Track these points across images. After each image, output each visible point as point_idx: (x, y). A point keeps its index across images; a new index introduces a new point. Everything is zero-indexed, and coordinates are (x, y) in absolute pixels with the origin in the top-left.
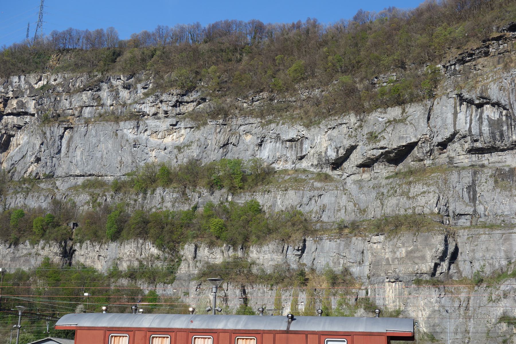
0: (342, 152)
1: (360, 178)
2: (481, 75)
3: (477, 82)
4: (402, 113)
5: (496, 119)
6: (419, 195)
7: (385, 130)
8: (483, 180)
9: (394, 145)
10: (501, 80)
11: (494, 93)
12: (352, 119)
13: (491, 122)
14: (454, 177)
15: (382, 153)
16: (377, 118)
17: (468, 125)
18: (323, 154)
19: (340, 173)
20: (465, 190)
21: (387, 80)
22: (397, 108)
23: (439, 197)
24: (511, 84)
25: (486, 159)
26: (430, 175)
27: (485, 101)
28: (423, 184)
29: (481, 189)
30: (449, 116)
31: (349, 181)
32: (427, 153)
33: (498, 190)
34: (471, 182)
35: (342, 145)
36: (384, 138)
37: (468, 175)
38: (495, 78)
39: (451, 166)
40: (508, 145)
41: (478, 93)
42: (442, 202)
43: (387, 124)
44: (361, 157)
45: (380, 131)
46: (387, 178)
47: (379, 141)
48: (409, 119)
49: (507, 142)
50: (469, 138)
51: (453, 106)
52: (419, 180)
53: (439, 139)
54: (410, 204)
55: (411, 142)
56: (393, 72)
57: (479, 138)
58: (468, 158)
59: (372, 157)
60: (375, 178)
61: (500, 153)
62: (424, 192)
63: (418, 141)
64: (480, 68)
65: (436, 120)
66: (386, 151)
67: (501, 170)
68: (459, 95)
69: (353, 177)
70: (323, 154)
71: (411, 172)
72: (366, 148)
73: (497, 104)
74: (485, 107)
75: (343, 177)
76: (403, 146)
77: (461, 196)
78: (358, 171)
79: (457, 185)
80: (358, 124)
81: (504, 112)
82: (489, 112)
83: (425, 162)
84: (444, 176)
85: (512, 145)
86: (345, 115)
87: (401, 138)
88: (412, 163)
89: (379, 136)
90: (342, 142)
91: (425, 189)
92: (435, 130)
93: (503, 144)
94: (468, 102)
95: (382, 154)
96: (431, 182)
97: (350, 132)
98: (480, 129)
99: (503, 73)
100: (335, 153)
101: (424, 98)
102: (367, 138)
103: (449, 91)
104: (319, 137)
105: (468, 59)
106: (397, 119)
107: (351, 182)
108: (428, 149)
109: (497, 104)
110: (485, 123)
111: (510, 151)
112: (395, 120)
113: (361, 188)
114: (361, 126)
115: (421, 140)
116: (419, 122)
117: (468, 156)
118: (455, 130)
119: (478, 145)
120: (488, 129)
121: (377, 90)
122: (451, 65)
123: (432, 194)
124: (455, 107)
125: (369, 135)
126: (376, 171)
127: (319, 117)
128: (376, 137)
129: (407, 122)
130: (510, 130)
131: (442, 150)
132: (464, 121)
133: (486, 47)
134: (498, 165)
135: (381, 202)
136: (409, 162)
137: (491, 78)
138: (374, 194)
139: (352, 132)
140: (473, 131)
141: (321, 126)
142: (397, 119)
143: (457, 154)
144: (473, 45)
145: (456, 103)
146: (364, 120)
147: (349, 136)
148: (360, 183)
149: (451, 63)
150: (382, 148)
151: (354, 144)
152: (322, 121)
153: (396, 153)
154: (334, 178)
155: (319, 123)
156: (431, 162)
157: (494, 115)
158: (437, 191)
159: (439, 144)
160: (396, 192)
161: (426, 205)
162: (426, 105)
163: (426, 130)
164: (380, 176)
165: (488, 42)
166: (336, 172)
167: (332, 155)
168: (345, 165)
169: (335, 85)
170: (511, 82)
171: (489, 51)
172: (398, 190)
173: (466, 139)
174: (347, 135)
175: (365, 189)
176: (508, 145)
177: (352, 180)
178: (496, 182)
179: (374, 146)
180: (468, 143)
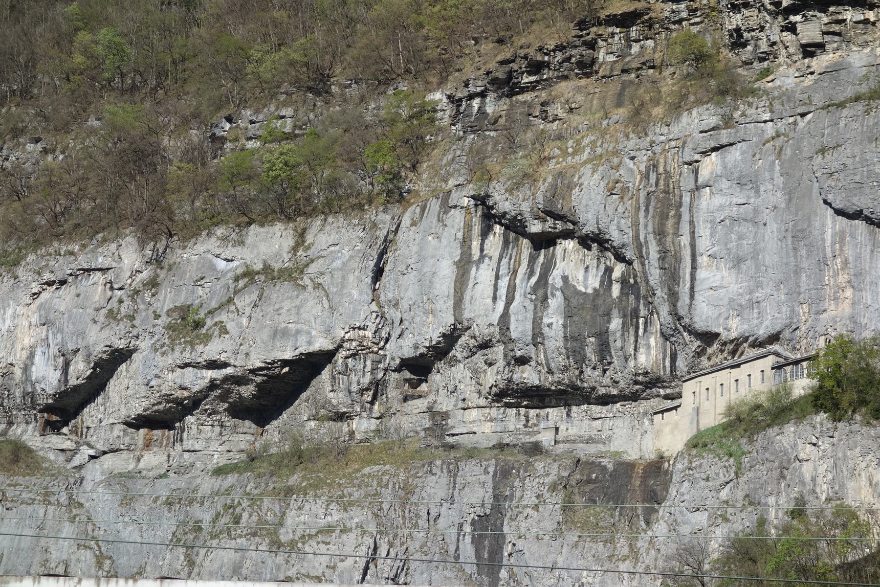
0: (80, 369)
1: (131, 467)
2: (560, 137)
3: (544, 160)
4: (295, 249)
5: (590, 291)
6: (310, 536)
7: (230, 301)
8: (530, 498)
9: (253, 356)
10: (616, 160)
11: (590, 204)
12: (127, 256)
13: (574, 302)
14: (435, 486)
15: (212, 381)
16: (212, 258)
17: (501, 305)
18: (18, 372)
19: (68, 445)
20: (468, 528)
21: (260, 132)
22: (279, 226)
23: (375, 549)
24: (647, 177)
25: (559, 426)
26: (358, 471)
27: (560, 226)
29: (518, 528)
30: (438, 269)
31: (94, 473)
32: (362, 391)
33: (572, 537)
34: (489, 501)
35: (81, 344)
36: (224, 331)
37: (483, 478)
38: (599, 150)
39: (436, 443)
40: (622, 384)
41: (540, 199)
43: (241, 283)
44: (143, 390)
45: (214, 304)
46: (219, 471)
47: (207, 339)
48: (312, 269)
49: (620, 375)
50: (499, 349)
51: (460, 235)
52: (316, 487)
53: (404, 347)
54: (278, 568)
56: (285, 104)
57: (531, 351)
58: (492, 420)
59: (179, 394)
60: (182, 470)
61: (596, 409)
62: (329, 530)
64: (560, 113)
65: (403, 280)
66: (227, 379)
67: (592, 465)
68: (481, 200)
69: (108, 461)
70: (18, 372)
71: (298, 457)
73: (593, 241)
74: (559, 249)
75: (77, 461)
76: (285, 363)
77: (452, 549)
78: (127, 440)
79: (443, 510)
80: (145, 275)
81: (619, 270)
82: (572, 265)
83: (354, 424)
84: (402, 477)
85: (636, 383)
86: (104, 240)
87: (279, 334)
88: (312, 423)
89: (209, 322)
90: (82, 334)
91: (335, 516)
92: (394, 314)
93: (606, 380)
94: (507, 228)
95: (213, 385)
96: (356, 495)
97: (115, 300)
98: (537, 323)
99: (627, 136)
100: (58, 373)
101: (370, 202)
102: (169, 327)
103: (452, 182)
104: (10, 312)
105: (526, 79)
106: (277, 266)
107: (99, 477)
108: (366, 380)
109: (593, 241)
110: (556, 302)
111: (630, 406)
112: (267, 269)
113: (128, 500)
114: (153, 284)
115: (346, 345)
116: (343, 284)
117: (494, 412)
119: (529, 376)
120: (561, 322)
121: (225, 160)
122: (471, 97)
123: (352, 535)
124: (465, 242)
125: (176, 315)
126: (188, 444)
127: (20, 239)
128: (198, 325)
129: (306, 281)
130: (632, 331)
131: (414, 385)
132: (490, 291)
133: (585, 43)
134: (584, 451)
135: (187, 556)
136: (300, 418)
137: (588, 150)
138: (167, 527)
139: (121, 301)
140: (512, 327)
141: (20, 272)
142: (277, 266)
143: (461, 404)
144: (548, 34)
145: (468, 227)
146: (166, 263)
147: (112, 315)
148: (129, 484)
149: (472, 89)
150: (213, 365)
151: (121, 344)
152: (26, 255)
153: (258, 385)
154: (45, 459)
155: (16, 263)
156: (374, 424)
157: (586, 278)
158: (372, 527)
159: (406, 364)
160: (237, 520)
161: (328, 572)
162: (375, 226)
163: (365, 314)
164: (199, 465)
165: (594, 29)
166: (56, 441)
167: (47, 377)
168: (91, 414)
169: (93, 131)
170: (648, 169)
171: (594, 61)
172: (245, 515)
173: (491, 354)
174: (104, 312)
175: (141, 507)
176: (622, 384)
177: (102, 473)
178: (567, 508)
179: (187, 357)
180: (495, 367)
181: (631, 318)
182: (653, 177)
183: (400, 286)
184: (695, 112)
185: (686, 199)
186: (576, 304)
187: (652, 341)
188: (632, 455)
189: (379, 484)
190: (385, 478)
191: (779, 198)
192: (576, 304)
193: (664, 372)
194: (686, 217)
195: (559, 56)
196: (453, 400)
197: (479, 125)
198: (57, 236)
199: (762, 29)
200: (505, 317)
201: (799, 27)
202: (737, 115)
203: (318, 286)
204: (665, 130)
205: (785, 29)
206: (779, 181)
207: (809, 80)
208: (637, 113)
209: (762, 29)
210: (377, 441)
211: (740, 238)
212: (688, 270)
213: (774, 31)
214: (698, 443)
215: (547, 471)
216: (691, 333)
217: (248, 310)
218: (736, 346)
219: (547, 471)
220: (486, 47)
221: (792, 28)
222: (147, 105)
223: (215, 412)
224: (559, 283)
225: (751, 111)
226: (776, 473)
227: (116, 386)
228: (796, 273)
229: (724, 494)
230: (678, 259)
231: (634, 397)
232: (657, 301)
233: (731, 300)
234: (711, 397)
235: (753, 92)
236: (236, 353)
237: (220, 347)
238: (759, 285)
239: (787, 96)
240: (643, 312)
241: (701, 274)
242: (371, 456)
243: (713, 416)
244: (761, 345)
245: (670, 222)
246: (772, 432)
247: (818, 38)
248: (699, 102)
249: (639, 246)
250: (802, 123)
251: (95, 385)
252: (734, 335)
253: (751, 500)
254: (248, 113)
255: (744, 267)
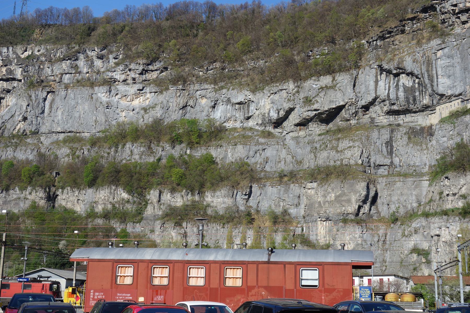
0: (282, 113)
2: (398, 49)
4: (333, 81)
8: (399, 137)
9: (325, 107)
10: (414, 54)
11: (409, 65)
12: (291, 86)
14: (375, 134)
16: (312, 85)
17: (387, 91)
18: (267, 115)
19: (280, 131)
20: (384, 145)
21: (320, 53)
25: (401, 119)
27: (401, 71)
28: (350, 140)
30: (371, 83)
31: (288, 137)
32: (353, 114)
33: (411, 145)
36: (317, 102)
38: (409, 52)
40: (419, 108)
42: (365, 155)
43: (320, 90)
44: (298, 117)
45: (314, 96)
46: (320, 135)
47: (313, 104)
48: (338, 85)
49: (419, 106)
52: (346, 137)
53: (363, 102)
54: (339, 157)
55: (340, 105)
56: (325, 46)
57: (396, 102)
59: (307, 117)
60: (310, 135)
61: (413, 115)
62: (350, 147)
63: (346, 105)
64: (398, 43)
65: (361, 87)
66: (319, 113)
68: (380, 66)
69: (291, 134)
70: (267, 115)
72: (302, 110)
73: (411, 74)
74: (401, 76)
76: (333, 108)
77: (380, 150)
80: (296, 90)
81: (417, 81)
82: (405, 80)
83: (351, 122)
84: (366, 134)
86: (285, 82)
87: (331, 102)
89: (313, 100)
90: (282, 105)
91: (351, 144)
93: (415, 107)
94: (387, 72)
96: (356, 139)
98: (397, 95)
100: (277, 114)
101: (351, 68)
102: (303, 102)
103: (371, 62)
104: (263, 101)
105: (387, 36)
106: (329, 85)
107: (289, 138)
108: (354, 111)
110: (401, 89)
111: (421, 113)
112: (326, 86)
113: (298, 143)
114: (298, 92)
117: (387, 117)
118: (376, 95)
119: (395, 108)
122: (373, 41)
123: (356, 148)
124: (376, 76)
126: (310, 129)
128: (311, 101)
129: (337, 88)
130: (421, 95)
131: (365, 111)
132: (384, 88)
135: (314, 155)
138: (309, 148)
139: (290, 97)
141: (264, 91)
142: (329, 85)
144: (392, 24)
145: (377, 73)
148: (298, 139)
149: (373, 39)
150: (315, 110)
151: (292, 107)
153: (327, 114)
155: (263, 89)
156: (356, 121)
157: (409, 83)
158: (361, 146)
159: (363, 107)
160: (327, 146)
161: (351, 157)
162: (352, 74)
163: (352, 95)
165: (404, 22)
166: (277, 130)
167: (274, 116)
168: (285, 124)
169: (276, 57)
171: (405, 30)
172: (329, 145)
173: (385, 103)
174: (287, 99)
175: (301, 144)
176: (419, 108)
178: (409, 138)
179: (309, 108)
181: (421, 92)
182: (424, 57)
183: (361, 88)
184: (434, 41)
185: (434, 62)
186: (406, 90)
187: (427, 97)
188: (424, 125)
189: (361, 135)
190: (362, 134)
191: (459, 60)
192: (406, 90)
193: (430, 104)
194: (434, 66)
195: (395, 29)
196: (376, 115)
197: (376, 47)
198: (273, 82)
199: (450, 18)
200: (388, 94)
201: (461, 17)
202: (446, 40)
203: (340, 90)
204: (427, 45)
205: (456, 18)
206: (459, 56)
207: (464, 30)
208: (418, 41)
209: (450, 18)
210: (357, 126)
211: (449, 71)
212: (436, 79)
213: (453, 19)
214: (442, 121)
215: (403, 130)
216: (437, 94)
217: (323, 97)
218: (450, 97)
219: (403, 130)
220: (376, 28)
221: (459, 18)
222: (289, 49)
223: (316, 121)
224: (402, 85)
225: (449, 39)
226: (465, 127)
227: (291, 117)
228: (465, 78)
229: (451, 133)
230: (433, 77)
231: (423, 111)
232: (427, 87)
233: (448, 86)
234: (444, 110)
235: (450, 34)
236: (321, 107)
237: (317, 106)
238: (455, 82)
239: (459, 35)
240: (424, 90)
241: (439, 80)
242: (357, 129)
243: (446, 114)
244: (457, 96)
245: (430, 68)
246: (463, 117)
247: (466, 19)
248: (435, 38)
249: (422, 74)
250: (464, 41)
251: (286, 117)
252: (449, 94)
253: (459, 134)
254: (316, 49)
255: (451, 78)
